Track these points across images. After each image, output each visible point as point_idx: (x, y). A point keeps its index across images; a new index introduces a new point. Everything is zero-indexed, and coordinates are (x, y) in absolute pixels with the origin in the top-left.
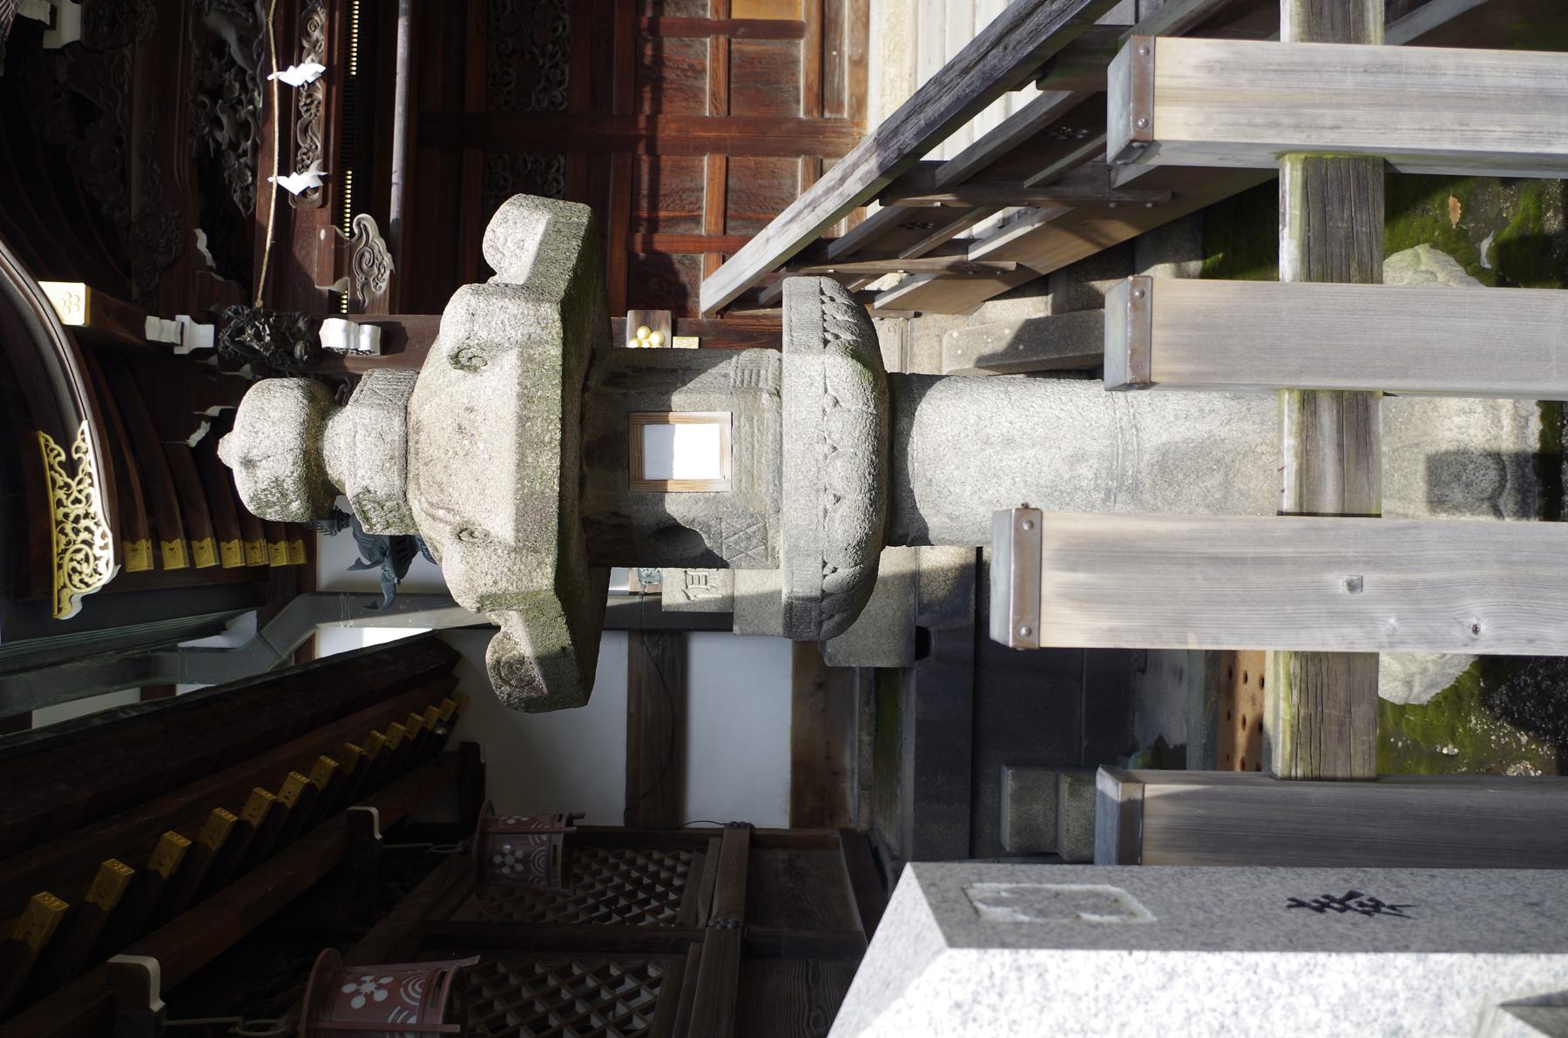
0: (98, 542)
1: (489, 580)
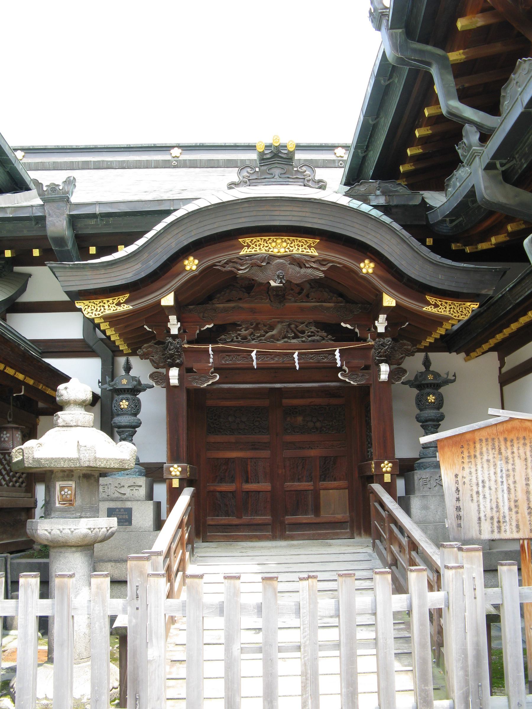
0: (97, 313)
1: (27, 452)
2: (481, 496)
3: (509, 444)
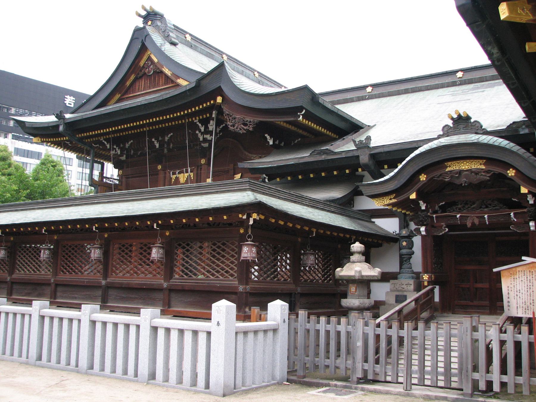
2: (518, 297)
3: (531, 274)
